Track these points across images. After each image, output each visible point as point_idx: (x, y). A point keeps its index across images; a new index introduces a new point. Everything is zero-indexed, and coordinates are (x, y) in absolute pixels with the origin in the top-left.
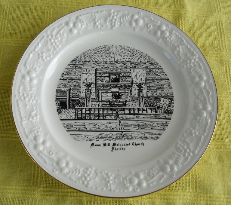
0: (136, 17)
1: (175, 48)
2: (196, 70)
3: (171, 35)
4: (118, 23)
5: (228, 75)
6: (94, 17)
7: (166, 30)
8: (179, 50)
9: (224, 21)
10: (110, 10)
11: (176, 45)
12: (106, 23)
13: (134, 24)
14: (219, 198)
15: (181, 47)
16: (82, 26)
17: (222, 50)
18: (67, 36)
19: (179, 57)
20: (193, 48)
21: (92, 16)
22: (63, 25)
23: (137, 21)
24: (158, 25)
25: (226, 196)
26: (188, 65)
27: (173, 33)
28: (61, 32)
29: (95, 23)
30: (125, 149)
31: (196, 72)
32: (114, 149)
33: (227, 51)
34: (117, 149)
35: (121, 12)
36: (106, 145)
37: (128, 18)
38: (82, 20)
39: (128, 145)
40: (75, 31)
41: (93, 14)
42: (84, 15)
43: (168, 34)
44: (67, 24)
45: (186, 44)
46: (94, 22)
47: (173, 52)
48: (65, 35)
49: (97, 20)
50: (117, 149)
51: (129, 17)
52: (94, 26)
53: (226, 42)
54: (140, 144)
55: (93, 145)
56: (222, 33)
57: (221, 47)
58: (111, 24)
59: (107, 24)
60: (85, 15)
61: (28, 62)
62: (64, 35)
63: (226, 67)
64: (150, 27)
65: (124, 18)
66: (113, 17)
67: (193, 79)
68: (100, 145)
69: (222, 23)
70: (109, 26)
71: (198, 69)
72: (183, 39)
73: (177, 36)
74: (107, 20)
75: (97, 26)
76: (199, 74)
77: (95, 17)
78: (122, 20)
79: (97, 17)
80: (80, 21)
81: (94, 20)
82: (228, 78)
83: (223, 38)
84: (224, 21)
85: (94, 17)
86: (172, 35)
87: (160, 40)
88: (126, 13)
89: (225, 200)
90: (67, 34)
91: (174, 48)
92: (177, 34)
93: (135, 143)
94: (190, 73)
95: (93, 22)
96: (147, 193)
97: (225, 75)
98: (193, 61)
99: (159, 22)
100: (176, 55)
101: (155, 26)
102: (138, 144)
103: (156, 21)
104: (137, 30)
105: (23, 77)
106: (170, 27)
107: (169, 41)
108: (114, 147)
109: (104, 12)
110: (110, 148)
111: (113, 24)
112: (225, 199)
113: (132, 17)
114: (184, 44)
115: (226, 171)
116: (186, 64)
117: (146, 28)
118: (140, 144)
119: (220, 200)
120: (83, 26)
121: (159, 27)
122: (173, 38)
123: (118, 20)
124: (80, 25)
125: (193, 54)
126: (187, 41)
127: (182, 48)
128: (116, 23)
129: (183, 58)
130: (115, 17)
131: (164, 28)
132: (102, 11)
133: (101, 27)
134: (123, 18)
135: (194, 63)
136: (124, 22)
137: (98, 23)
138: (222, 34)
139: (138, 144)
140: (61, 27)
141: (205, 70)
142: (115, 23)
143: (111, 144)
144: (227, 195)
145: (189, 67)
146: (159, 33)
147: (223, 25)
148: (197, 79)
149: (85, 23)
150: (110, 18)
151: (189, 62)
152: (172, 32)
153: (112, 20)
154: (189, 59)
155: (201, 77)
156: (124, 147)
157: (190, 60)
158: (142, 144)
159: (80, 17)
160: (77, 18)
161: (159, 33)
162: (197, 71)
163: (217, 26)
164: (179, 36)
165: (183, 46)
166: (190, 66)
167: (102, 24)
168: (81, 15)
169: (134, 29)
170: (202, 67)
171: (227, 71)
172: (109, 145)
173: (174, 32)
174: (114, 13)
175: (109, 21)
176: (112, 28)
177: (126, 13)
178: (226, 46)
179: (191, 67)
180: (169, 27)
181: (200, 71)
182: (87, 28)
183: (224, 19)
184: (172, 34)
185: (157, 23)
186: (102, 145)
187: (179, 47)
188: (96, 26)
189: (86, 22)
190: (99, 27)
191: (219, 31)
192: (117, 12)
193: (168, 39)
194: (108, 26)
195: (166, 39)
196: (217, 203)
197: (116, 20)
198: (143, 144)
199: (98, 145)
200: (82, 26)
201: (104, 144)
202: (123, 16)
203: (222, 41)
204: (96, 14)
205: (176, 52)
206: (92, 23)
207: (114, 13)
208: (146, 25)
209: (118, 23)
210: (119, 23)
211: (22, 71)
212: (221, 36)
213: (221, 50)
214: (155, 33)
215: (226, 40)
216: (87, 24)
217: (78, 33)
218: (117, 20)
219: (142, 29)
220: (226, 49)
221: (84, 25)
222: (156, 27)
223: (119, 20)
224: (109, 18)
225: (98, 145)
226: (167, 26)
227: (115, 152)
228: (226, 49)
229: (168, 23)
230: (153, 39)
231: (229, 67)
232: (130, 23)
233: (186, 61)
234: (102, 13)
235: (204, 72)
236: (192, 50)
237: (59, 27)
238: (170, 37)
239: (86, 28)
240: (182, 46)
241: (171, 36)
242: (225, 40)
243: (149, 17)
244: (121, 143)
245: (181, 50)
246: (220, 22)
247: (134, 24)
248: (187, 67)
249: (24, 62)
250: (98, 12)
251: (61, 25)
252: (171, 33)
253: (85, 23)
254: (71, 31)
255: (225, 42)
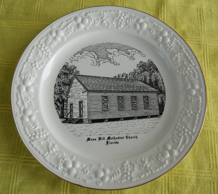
0: (142, 20)
1: (174, 54)
2: (190, 78)
3: (172, 41)
4: (124, 24)
5: (205, 59)
6: (103, 15)
7: (168, 36)
8: (177, 57)
9: (204, 7)
10: (118, 11)
11: (175, 51)
12: (113, 22)
13: (138, 26)
14: (189, 172)
15: (179, 54)
16: (89, 22)
17: (201, 35)
18: (74, 31)
19: (176, 63)
20: (191, 57)
21: (100, 14)
22: (72, 19)
23: (141, 25)
24: (161, 30)
25: (196, 170)
26: (184, 72)
27: (174, 40)
28: (69, 26)
29: (102, 22)
30: (118, 143)
31: (189, 80)
32: (109, 142)
33: (205, 36)
34: (111, 143)
35: (129, 14)
36: (101, 139)
37: (134, 21)
38: (90, 17)
39: (122, 138)
40: (82, 26)
41: (102, 13)
42: (93, 14)
43: (169, 40)
44: (76, 19)
45: (185, 52)
46: (102, 20)
47: (172, 58)
48: (72, 29)
49: (104, 18)
50: (111, 143)
51: (135, 19)
52: (101, 24)
53: (205, 27)
54: (134, 137)
55: (89, 139)
56: (202, 19)
57: (200, 32)
58: (117, 24)
59: (114, 23)
60: (94, 13)
61: (22, 72)
62: (71, 28)
63: (204, 50)
64: (153, 32)
65: (130, 20)
66: (120, 18)
67: (186, 85)
68: (96, 139)
69: (202, 10)
70: (115, 25)
71: (192, 77)
72: (183, 47)
73: (177, 43)
74: (114, 20)
75: (104, 24)
76: (192, 82)
77: (104, 15)
78: (127, 22)
79: (105, 16)
80: (88, 17)
81: (102, 18)
82: (205, 61)
83: (202, 23)
84: (205, 7)
85: (103, 15)
86: (173, 42)
87: (161, 46)
88: (133, 16)
89: (195, 174)
90: (75, 28)
91: (173, 54)
92: (178, 41)
93: (128, 136)
94: (183, 80)
95: (101, 20)
96: (133, 186)
97: (203, 58)
98: (189, 69)
99: (162, 28)
100: (174, 61)
101: (157, 31)
102: (131, 138)
103: (159, 27)
104: (141, 33)
105: (19, 88)
106: (172, 34)
107: (170, 47)
108: (109, 140)
109: (113, 11)
110: (105, 142)
111: (119, 24)
112: (194, 174)
113: (138, 20)
114: (183, 51)
115: (197, 147)
116: (182, 72)
117: (149, 33)
118: (134, 137)
119: (190, 174)
120: (91, 23)
121: (161, 33)
122: (174, 43)
123: (125, 21)
124: (87, 21)
125: (190, 62)
126: (186, 50)
127: (180, 55)
128: (122, 23)
129: (180, 65)
130: (122, 18)
131: (166, 34)
132: (110, 11)
133: (108, 25)
134: (129, 20)
135: (189, 71)
136: (129, 23)
137: (105, 21)
138: (201, 20)
139: (131, 138)
140: (69, 21)
141: (199, 79)
142: (121, 23)
143: (106, 138)
144: (197, 169)
145: (184, 74)
146: (161, 38)
147: (204, 12)
148: (190, 87)
149: (93, 20)
150: (117, 19)
151: (184, 69)
152: (173, 38)
153: (118, 21)
154: (185, 66)
155: (193, 87)
156: (117, 140)
157: (186, 68)
158: (135, 137)
159: (89, 14)
160: (86, 14)
161: (161, 38)
162: (191, 78)
163: (198, 13)
164: (180, 43)
165: (182, 54)
166: (185, 73)
167: (109, 22)
168: (90, 12)
169: (138, 31)
170: (197, 76)
171: (205, 54)
172: (104, 139)
173: (175, 38)
174: (121, 14)
175: (116, 20)
176: (117, 27)
177: (133, 16)
178: (205, 31)
179: (186, 75)
180: (171, 34)
181: (193, 79)
182: (94, 25)
183: (205, 6)
184: (173, 40)
185: (160, 28)
186: (98, 139)
187: (177, 54)
188: (103, 24)
189: (94, 19)
190: (106, 24)
191: (199, 17)
192: (125, 14)
193: (168, 45)
194: (114, 25)
195: (167, 45)
196: (155, 1)
197: (122, 20)
198: (137, 137)
199: (94, 140)
200: (89, 22)
201: (100, 139)
202: (131, 17)
203: (202, 27)
204: (104, 13)
205: (174, 59)
206: (100, 20)
207: (121, 14)
208: (149, 29)
209: (124, 24)
210: (125, 24)
211: (17, 82)
212: (201, 22)
213: (199, 35)
214: (157, 39)
215: (205, 25)
216: (94, 21)
217: (85, 29)
218: (124, 20)
219: (145, 33)
220: (205, 34)
221: (92, 21)
222: (159, 32)
223: (125, 21)
224: (116, 18)
225: (94, 140)
226: (169, 32)
227: (110, 145)
228: (205, 34)
229: (170, 30)
230: (155, 44)
231: (206, 51)
232: (135, 26)
233: (183, 68)
234: (110, 12)
235: (197, 81)
236: (190, 58)
237: (67, 21)
238: (170, 43)
239: (93, 24)
240: (180, 53)
241: (172, 43)
242: (204, 25)
243: (153, 23)
244: (116, 137)
245: (179, 57)
246: (201, 9)
247: (138, 26)
248: (182, 74)
249: (18, 74)
250: (107, 12)
251: (70, 19)
252: (172, 40)
253: (93, 20)
254: (78, 25)
255: (204, 27)
